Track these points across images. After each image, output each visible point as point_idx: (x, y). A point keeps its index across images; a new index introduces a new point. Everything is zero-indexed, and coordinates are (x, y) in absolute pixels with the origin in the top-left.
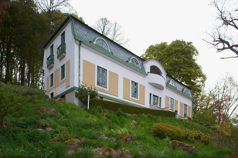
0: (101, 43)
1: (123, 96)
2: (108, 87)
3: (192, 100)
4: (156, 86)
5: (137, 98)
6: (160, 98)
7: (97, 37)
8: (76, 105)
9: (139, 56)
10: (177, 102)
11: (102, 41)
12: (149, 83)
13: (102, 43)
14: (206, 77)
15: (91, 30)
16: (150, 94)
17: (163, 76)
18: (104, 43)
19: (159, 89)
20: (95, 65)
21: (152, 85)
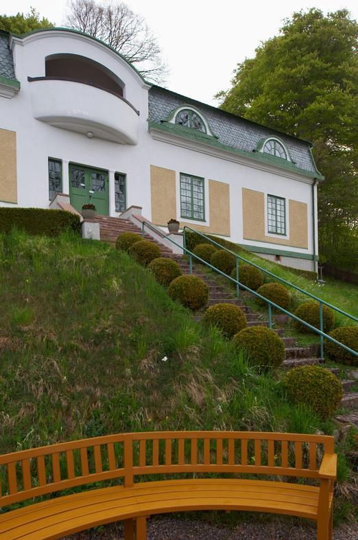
0: (273, 147)
1: (244, 233)
2: (207, 218)
3: (311, 181)
4: (67, 124)
5: (285, 235)
6: (120, 177)
7: (177, 109)
8: (20, 228)
9: (216, 104)
10: (221, 190)
11: (275, 144)
12: (45, 120)
13: (275, 146)
14: (291, 19)
15: (176, 99)
16: (54, 162)
17: (127, 99)
18: (279, 145)
19: (115, 144)
20: (263, 194)
21: (52, 126)
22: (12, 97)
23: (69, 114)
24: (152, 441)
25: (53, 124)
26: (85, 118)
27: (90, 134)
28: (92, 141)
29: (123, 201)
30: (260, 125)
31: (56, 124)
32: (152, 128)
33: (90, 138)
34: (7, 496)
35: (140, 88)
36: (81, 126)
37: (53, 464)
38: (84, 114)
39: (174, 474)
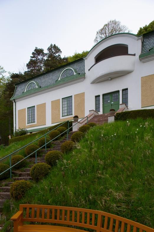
19: (125, 76)
21: (96, 83)
22: (84, 80)
23: (98, 76)
24: (92, 214)
25: (96, 82)
26: (104, 74)
27: (109, 79)
28: (112, 81)
29: (32, 122)
30: (41, 74)
31: (97, 82)
32: (141, 58)
33: (110, 80)
34: (36, 218)
35: (137, 41)
36: (100, 79)
37: (49, 212)
38: (103, 73)
39: (65, 225)
